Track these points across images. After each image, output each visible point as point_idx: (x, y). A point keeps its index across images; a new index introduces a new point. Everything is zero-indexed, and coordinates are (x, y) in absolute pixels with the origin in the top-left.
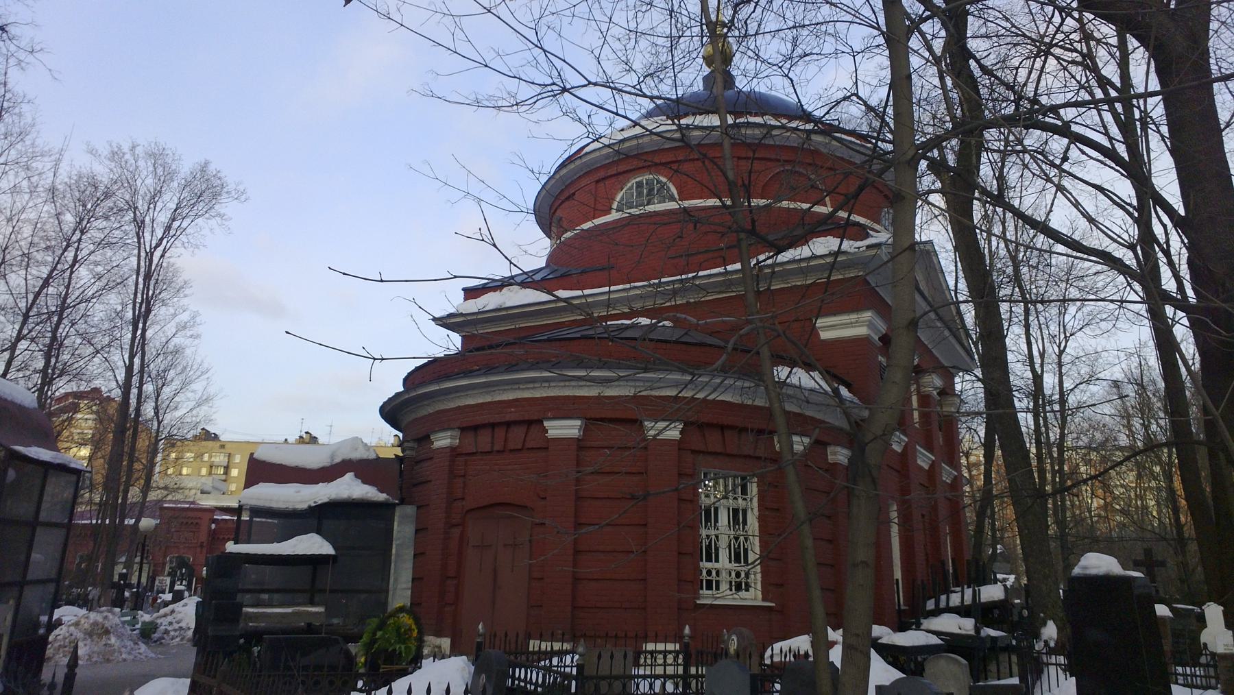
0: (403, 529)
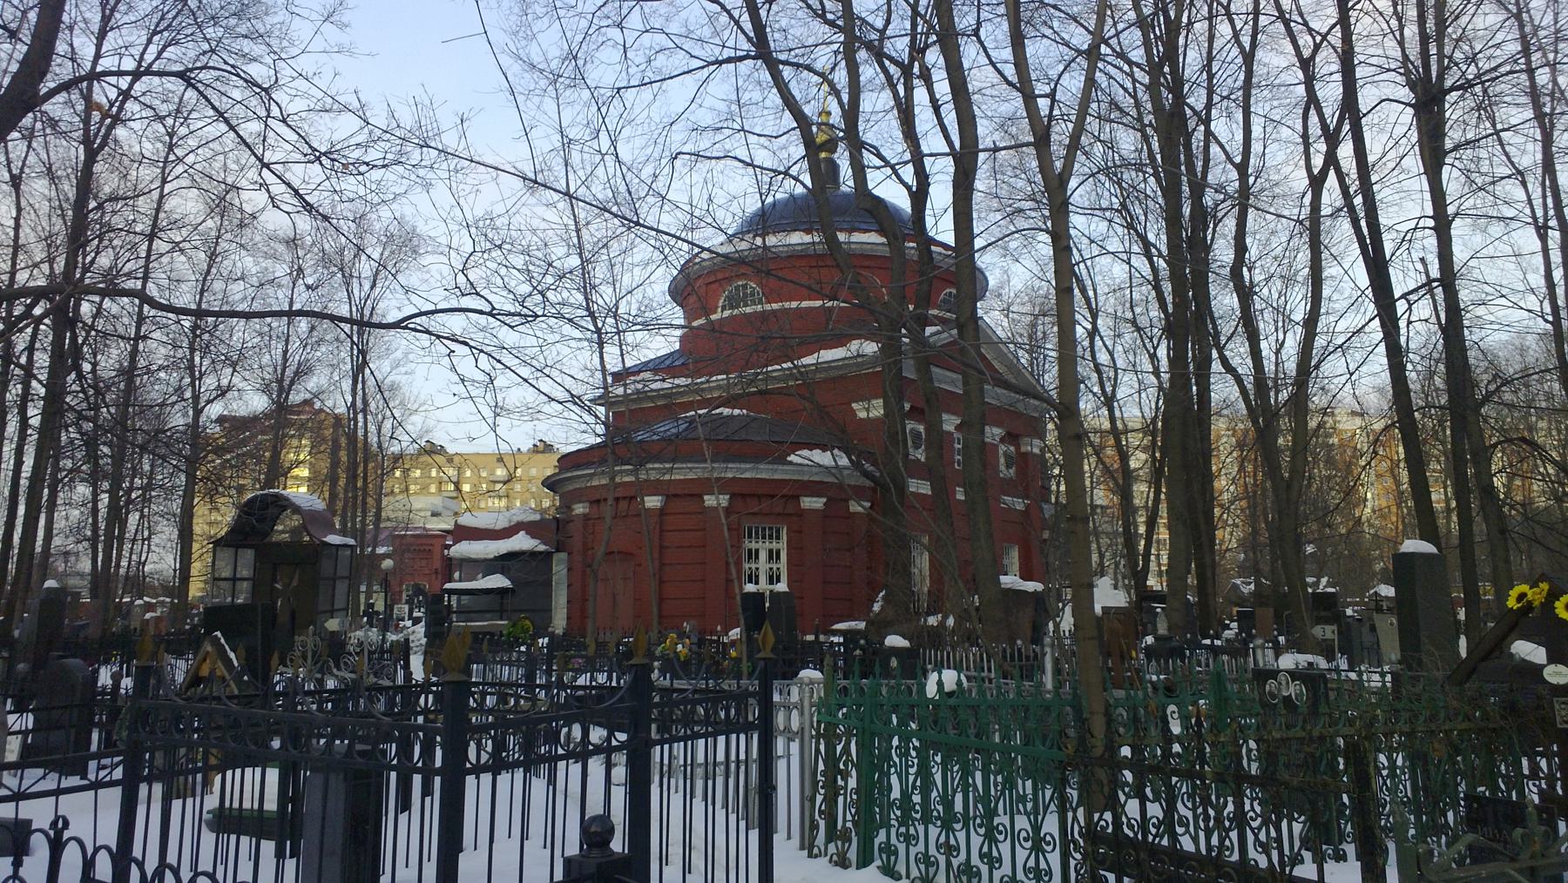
0: (559, 568)
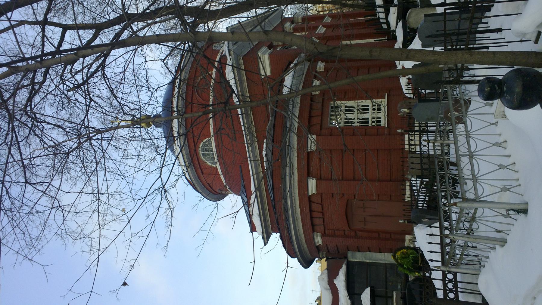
0: (358, 257)
